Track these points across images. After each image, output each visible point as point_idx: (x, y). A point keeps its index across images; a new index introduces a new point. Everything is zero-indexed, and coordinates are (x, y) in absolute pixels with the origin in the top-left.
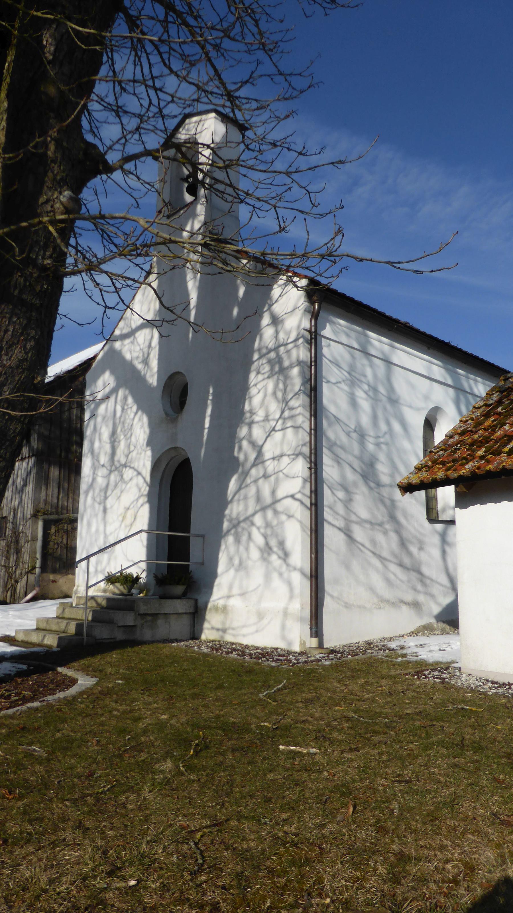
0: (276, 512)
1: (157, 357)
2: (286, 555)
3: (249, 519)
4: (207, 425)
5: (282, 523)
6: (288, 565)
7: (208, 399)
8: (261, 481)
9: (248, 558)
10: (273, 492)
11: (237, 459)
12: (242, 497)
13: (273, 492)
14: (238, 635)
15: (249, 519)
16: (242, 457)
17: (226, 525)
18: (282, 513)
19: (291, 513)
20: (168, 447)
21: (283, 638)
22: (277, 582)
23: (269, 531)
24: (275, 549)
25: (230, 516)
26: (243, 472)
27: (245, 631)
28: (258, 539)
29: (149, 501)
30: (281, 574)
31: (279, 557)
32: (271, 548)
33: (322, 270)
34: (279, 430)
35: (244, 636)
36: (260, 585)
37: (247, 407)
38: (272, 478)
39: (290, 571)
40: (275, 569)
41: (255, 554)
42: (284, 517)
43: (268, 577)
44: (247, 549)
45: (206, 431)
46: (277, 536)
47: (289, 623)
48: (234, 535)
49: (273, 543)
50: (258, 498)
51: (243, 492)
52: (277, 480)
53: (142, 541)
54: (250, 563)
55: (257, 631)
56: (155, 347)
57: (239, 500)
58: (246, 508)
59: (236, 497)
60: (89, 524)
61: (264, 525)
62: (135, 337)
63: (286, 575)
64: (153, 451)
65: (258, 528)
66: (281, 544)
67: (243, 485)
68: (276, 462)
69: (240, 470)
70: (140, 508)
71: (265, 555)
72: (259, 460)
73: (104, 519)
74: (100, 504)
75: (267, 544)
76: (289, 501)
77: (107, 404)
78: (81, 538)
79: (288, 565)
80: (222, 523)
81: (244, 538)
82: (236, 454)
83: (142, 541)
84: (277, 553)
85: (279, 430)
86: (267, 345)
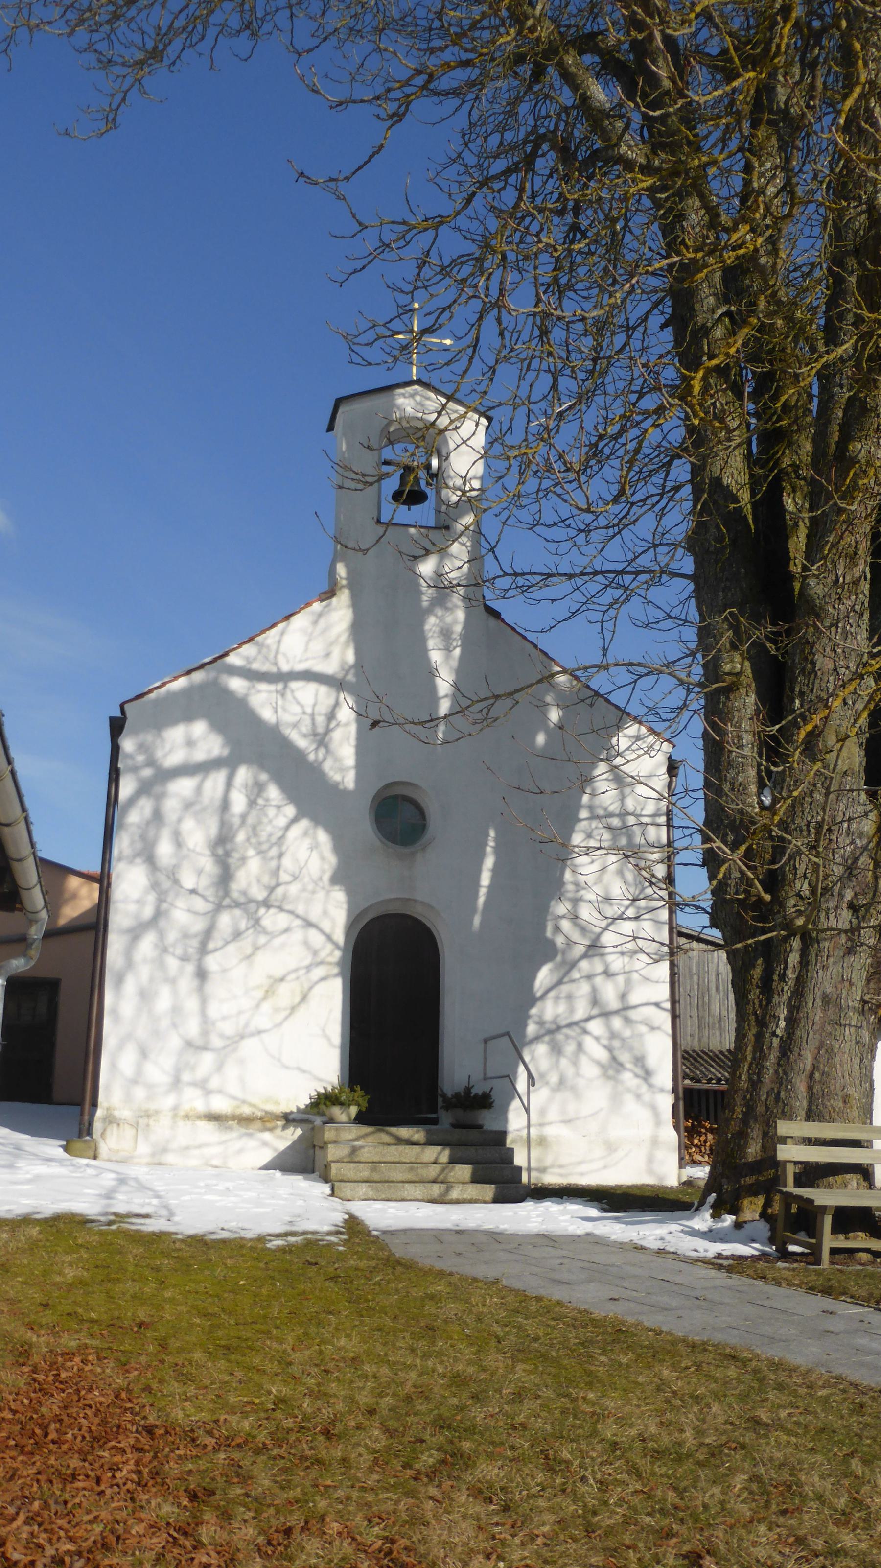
0: (628, 1021)
1: (353, 742)
2: (647, 1075)
3: (579, 1025)
4: (485, 879)
5: (641, 1035)
6: (651, 1086)
7: (486, 845)
8: (599, 980)
9: (578, 1074)
10: (623, 996)
11: (552, 944)
12: (563, 995)
13: (623, 996)
14: (570, 1174)
15: (579, 1025)
16: (560, 941)
17: (531, 1029)
18: (641, 1022)
19: (656, 1024)
20: (392, 896)
21: (650, 1172)
22: (630, 1104)
23: (616, 1043)
24: (629, 1065)
25: (540, 1017)
26: (564, 962)
27: (583, 1168)
28: (596, 1050)
29: (342, 974)
30: (638, 1097)
31: (637, 1076)
32: (621, 1065)
33: (439, 263)
34: (630, 919)
35: (582, 1174)
36: (601, 1109)
37: (568, 876)
38: (621, 979)
39: (654, 1093)
40: (629, 1090)
41: (589, 1070)
42: (643, 1029)
43: (616, 1100)
44: (575, 1063)
45: (483, 891)
46: (631, 1049)
47: (660, 1154)
48: (548, 1043)
49: (625, 1057)
50: (595, 1001)
51: (565, 989)
52: (628, 982)
53: (329, 1039)
54: (581, 1082)
55: (605, 1167)
56: (347, 724)
57: (557, 998)
58: (572, 1010)
59: (552, 994)
60: (145, 996)
61: (607, 1035)
62: (285, 687)
63: (647, 1097)
64: (351, 894)
65: (597, 1039)
66: (640, 1061)
67: (566, 980)
68: (626, 959)
69: (559, 958)
70: (317, 983)
71: (611, 1072)
72: (594, 948)
73: (200, 989)
74: (184, 959)
75: (614, 1059)
76: (653, 1009)
77: (203, 781)
78: (117, 1018)
79: (651, 1086)
80: (525, 1025)
81: (570, 1048)
82: (549, 933)
83: (329, 1039)
84: (631, 1071)
85: (630, 919)
86: (605, 805)
